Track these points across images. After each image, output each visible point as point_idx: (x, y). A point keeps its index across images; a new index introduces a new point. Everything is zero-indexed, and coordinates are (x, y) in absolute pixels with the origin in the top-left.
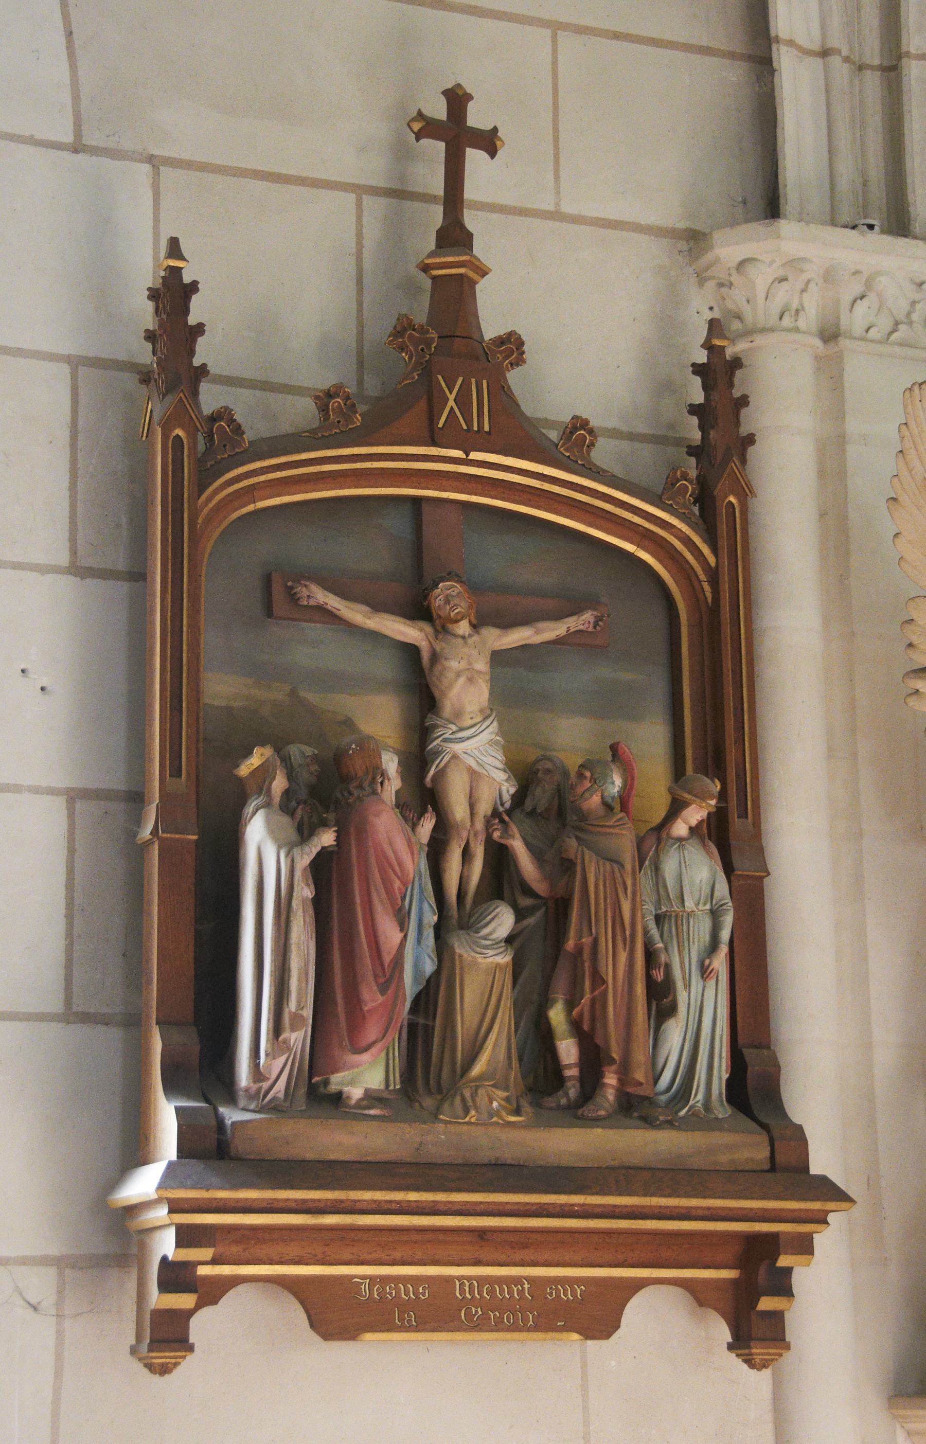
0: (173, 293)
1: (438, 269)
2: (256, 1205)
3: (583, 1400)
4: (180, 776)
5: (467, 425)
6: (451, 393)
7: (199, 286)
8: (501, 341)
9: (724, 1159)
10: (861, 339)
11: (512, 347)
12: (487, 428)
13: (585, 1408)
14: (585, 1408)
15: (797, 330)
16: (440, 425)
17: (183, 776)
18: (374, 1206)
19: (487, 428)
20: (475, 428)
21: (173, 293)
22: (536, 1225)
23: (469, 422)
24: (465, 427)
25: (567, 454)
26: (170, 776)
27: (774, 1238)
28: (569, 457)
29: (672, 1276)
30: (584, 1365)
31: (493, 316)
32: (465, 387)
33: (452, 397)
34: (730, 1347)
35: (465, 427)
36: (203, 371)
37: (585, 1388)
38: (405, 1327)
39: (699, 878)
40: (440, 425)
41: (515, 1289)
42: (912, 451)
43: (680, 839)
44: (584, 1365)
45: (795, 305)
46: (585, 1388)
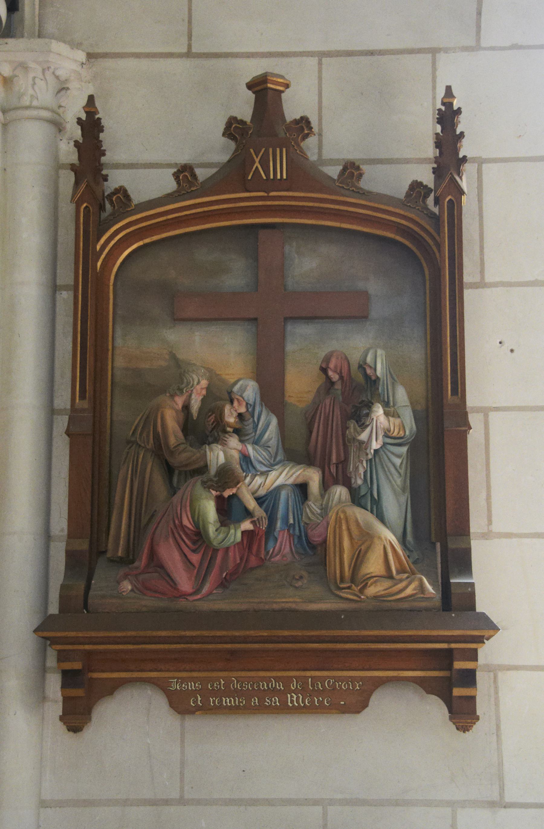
0: (91, 125)
1: (273, 84)
4: (457, 394)
5: (266, 175)
6: (257, 157)
7: (462, 110)
8: (296, 122)
11: (303, 126)
12: (285, 177)
16: (250, 178)
17: (459, 394)
19: (285, 177)
20: (272, 177)
21: (91, 125)
22: (422, 647)
23: (267, 173)
24: (265, 178)
26: (452, 395)
27: (450, 651)
31: (456, 105)
32: (266, 153)
33: (257, 160)
35: (265, 178)
36: (464, 159)
38: (316, 708)
40: (250, 178)
41: (358, 685)
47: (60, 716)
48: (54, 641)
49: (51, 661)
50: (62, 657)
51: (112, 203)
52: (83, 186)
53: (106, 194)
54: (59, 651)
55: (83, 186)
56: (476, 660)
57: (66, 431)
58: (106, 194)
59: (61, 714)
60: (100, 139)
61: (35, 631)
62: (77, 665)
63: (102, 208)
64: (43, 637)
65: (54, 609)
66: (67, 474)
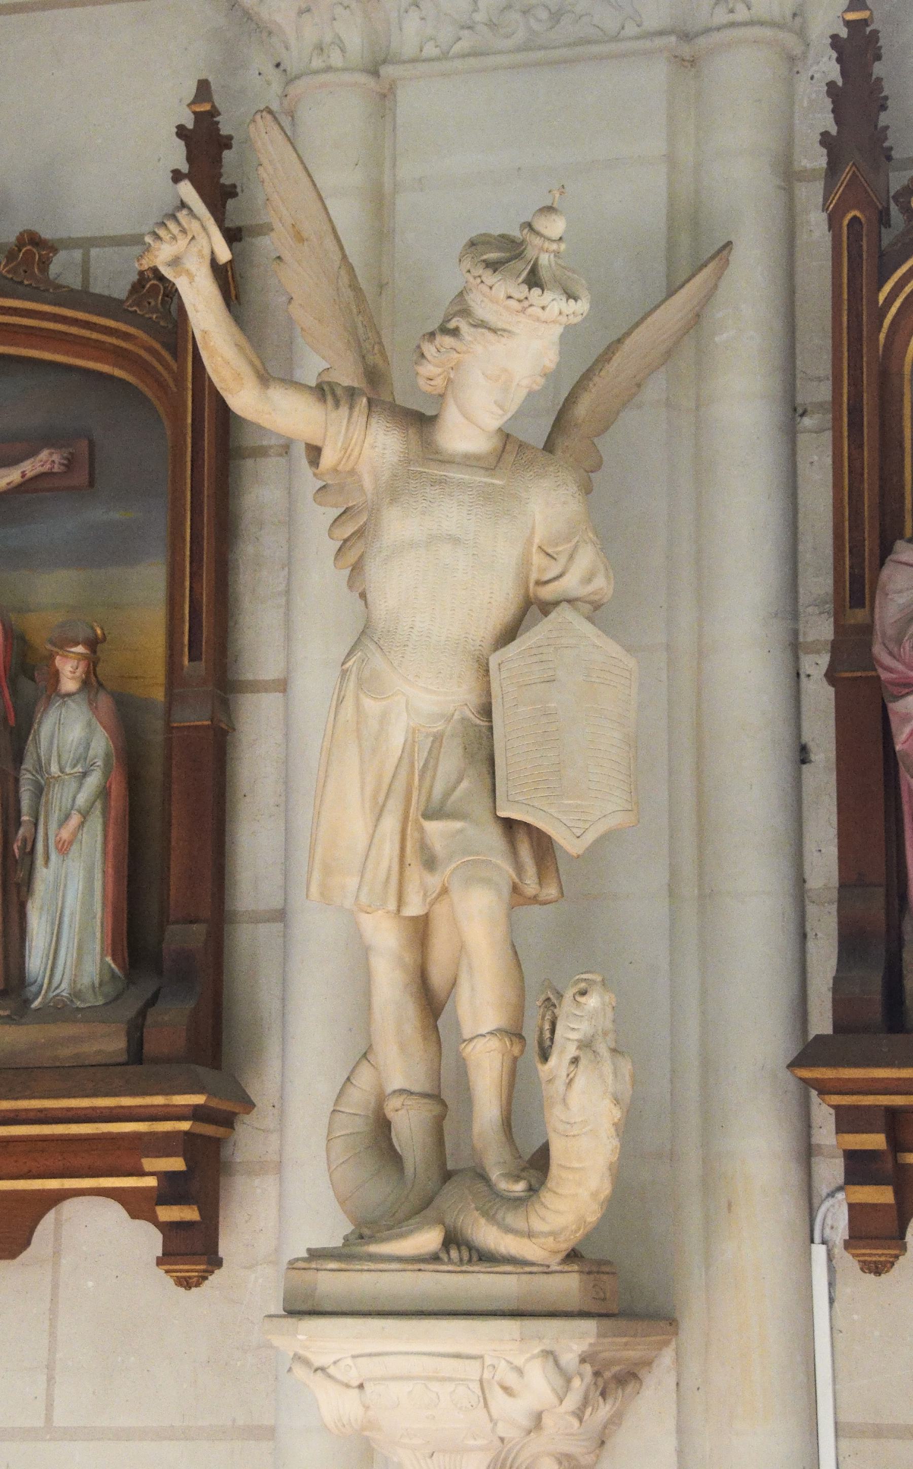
2: (23, 1116)
3: (51, 1325)
9: (66, 1052)
10: (414, 61)
13: (52, 1335)
14: (52, 1335)
15: (329, 69)
18: (42, 1115)
25: (10, 276)
28: (12, 279)
29: (128, 1185)
30: (55, 1286)
34: (160, 1262)
37: (53, 1313)
39: (71, 738)
42: (275, 196)
43: (69, 695)
44: (55, 1286)
45: (328, 38)
46: (53, 1313)
47: (158, 1258)
48: (824, 1088)
49: (825, 1132)
50: (847, 1120)
51: (905, 209)
52: (845, 176)
53: (892, 194)
54: (837, 1108)
55: (845, 176)
56: (851, 1207)
57: (827, 671)
58: (892, 194)
59: (160, 1254)
60: (224, 132)
61: (792, 1065)
62: (876, 1141)
63: (884, 218)
64: (801, 1079)
65: (822, 1023)
66: (833, 755)
